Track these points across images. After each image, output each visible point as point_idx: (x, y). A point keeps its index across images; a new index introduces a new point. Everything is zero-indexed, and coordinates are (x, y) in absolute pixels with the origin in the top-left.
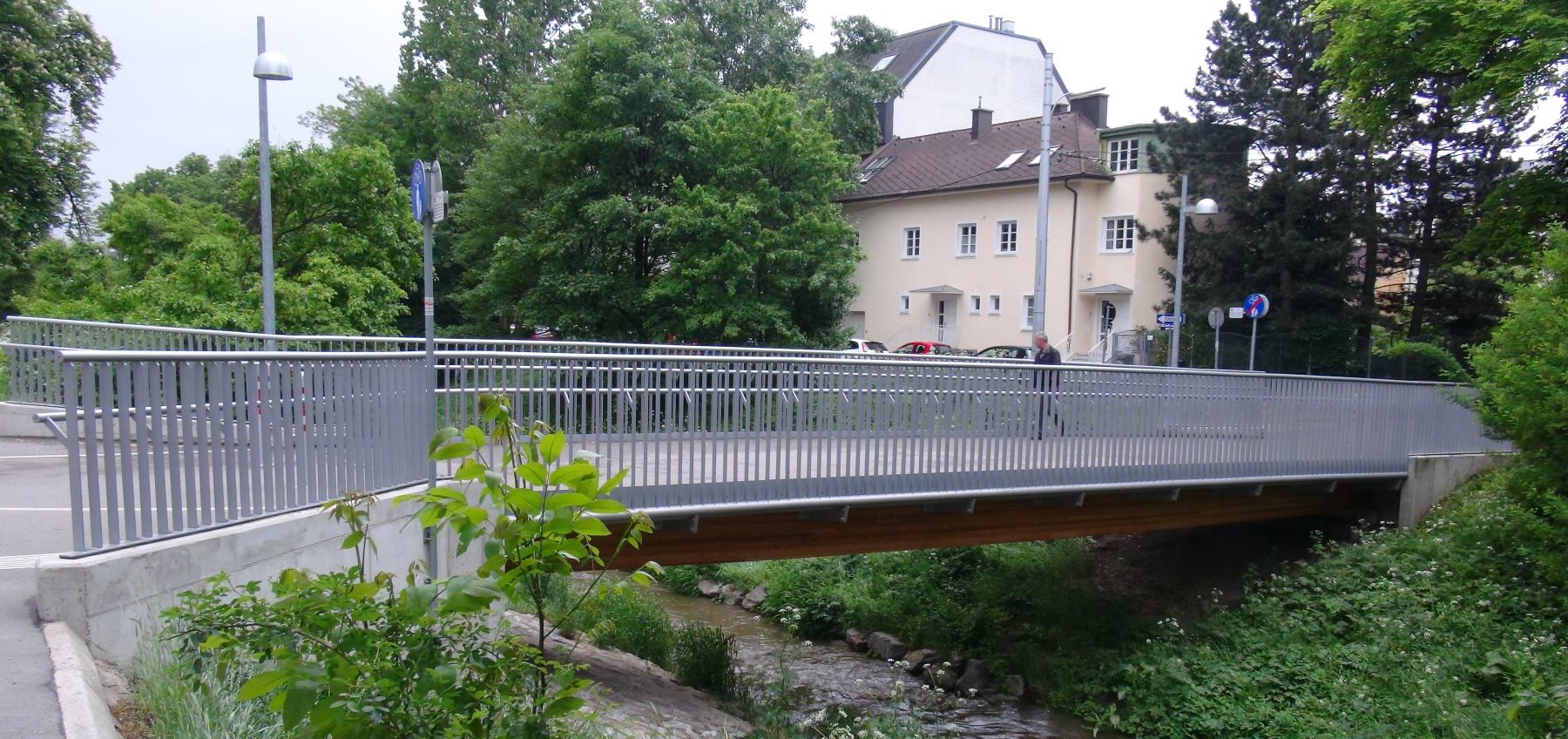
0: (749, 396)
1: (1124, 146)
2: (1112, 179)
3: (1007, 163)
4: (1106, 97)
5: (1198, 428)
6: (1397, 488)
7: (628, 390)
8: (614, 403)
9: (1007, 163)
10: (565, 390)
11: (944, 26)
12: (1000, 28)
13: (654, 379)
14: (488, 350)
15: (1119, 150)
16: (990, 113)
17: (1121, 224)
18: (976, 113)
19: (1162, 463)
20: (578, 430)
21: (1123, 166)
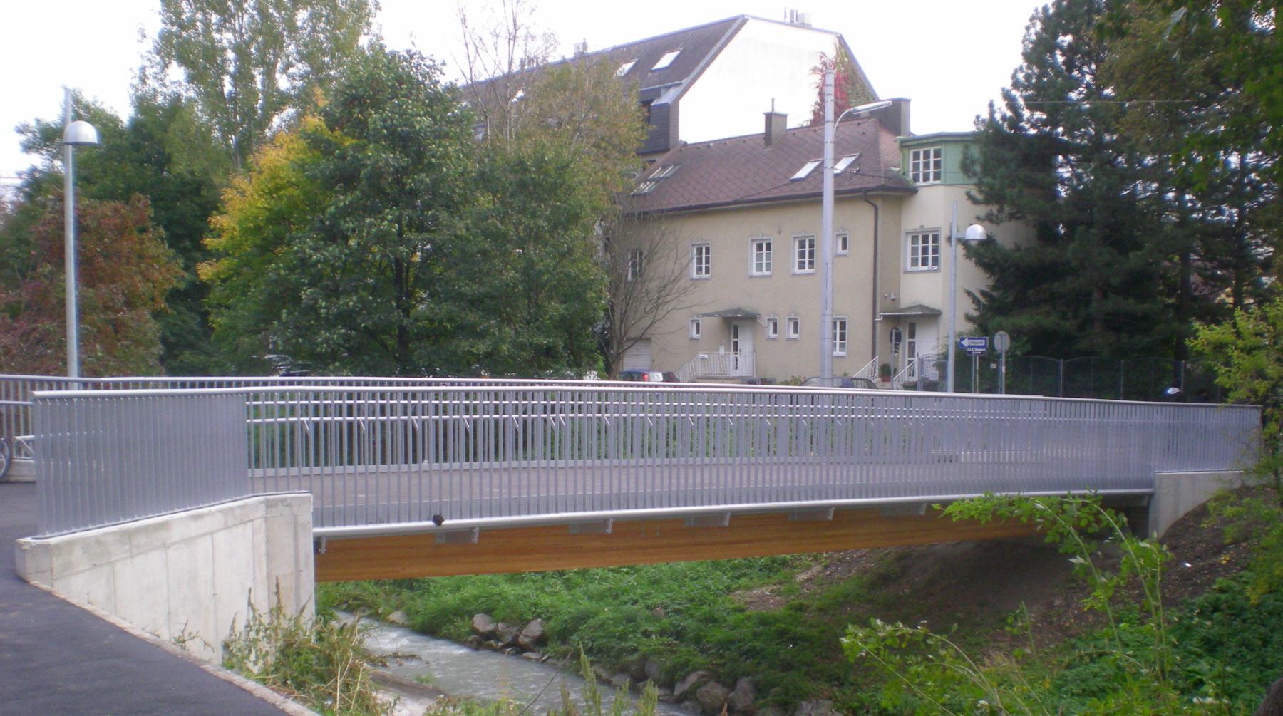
0: (472, 422)
1: (927, 155)
2: (914, 191)
3: (802, 173)
4: (907, 101)
5: (942, 451)
6: (1145, 504)
7: (305, 419)
8: (292, 433)
9: (802, 173)
10: (361, 418)
11: (734, 20)
12: (797, 22)
13: (392, 410)
14: (143, 388)
15: (922, 161)
16: (784, 117)
17: (925, 240)
18: (769, 117)
19: (864, 482)
20: (437, 461)
21: (926, 178)
